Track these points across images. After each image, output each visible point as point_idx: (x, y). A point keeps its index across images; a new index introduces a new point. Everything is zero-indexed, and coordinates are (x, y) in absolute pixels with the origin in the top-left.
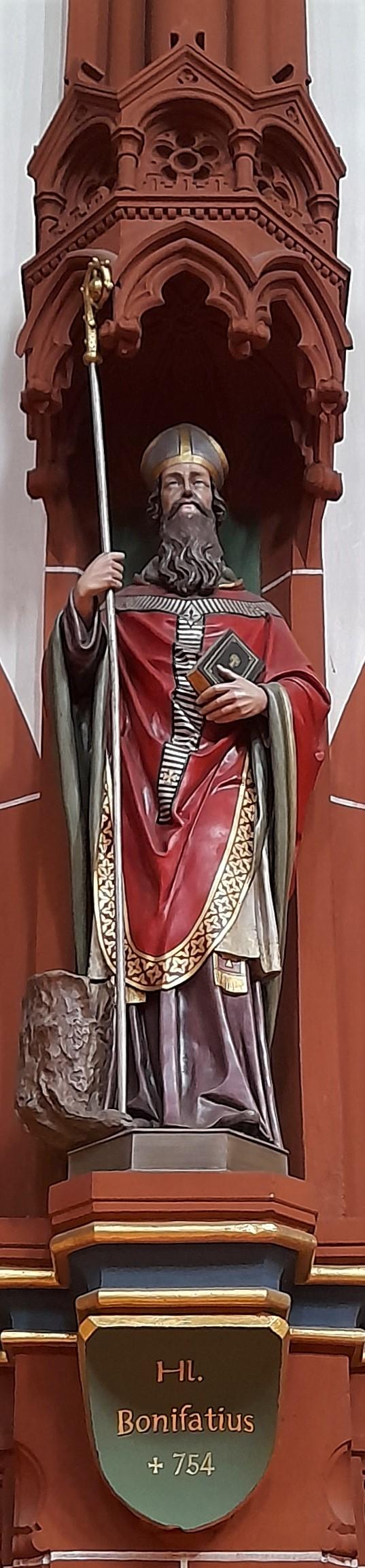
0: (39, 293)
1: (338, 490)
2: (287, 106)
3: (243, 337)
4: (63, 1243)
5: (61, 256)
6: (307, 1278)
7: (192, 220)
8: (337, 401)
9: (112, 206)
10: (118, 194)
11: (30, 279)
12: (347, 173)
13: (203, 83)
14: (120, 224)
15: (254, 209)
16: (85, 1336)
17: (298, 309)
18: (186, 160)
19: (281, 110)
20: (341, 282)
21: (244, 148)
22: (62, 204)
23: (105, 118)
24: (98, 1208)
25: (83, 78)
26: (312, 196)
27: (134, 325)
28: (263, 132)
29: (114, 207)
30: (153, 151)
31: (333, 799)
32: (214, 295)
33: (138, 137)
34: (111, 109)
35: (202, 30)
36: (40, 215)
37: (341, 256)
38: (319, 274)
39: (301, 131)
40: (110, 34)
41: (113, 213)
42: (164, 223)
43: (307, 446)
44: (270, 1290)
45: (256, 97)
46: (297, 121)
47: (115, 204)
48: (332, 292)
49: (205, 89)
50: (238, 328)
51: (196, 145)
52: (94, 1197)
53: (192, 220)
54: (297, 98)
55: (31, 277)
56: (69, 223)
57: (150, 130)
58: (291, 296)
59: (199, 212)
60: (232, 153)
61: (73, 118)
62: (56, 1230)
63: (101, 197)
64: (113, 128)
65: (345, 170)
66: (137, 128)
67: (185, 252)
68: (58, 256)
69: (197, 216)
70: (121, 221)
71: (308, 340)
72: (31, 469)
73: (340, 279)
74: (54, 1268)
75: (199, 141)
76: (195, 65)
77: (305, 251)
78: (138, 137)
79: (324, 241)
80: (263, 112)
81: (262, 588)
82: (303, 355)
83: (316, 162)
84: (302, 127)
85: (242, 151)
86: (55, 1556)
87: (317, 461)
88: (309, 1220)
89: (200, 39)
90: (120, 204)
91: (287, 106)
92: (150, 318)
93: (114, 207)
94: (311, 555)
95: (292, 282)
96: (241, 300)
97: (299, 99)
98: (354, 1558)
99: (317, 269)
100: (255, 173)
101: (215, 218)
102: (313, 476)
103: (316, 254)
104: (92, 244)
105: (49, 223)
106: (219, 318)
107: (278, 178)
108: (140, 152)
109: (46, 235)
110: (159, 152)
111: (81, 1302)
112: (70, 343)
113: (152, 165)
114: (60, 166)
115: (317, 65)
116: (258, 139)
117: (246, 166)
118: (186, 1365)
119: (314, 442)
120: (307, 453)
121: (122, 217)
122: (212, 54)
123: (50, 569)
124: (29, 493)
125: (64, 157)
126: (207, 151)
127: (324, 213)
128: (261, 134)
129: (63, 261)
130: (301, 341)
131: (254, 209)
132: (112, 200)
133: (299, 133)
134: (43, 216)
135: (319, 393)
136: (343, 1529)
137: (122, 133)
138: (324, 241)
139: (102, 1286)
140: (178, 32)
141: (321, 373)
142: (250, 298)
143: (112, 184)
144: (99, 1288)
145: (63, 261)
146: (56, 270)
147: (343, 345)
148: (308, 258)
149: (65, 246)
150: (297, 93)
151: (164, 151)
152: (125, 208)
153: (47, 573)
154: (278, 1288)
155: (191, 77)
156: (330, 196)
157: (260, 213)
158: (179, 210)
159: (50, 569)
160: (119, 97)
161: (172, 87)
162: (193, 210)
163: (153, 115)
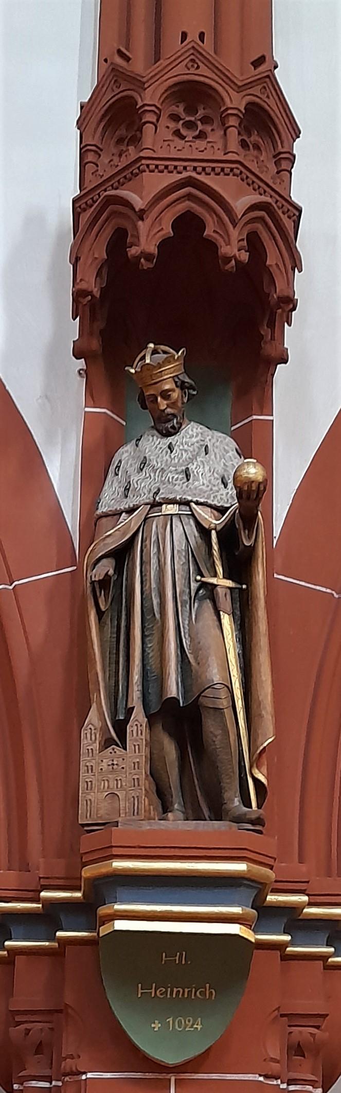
0: (85, 218)
1: (286, 358)
2: (260, 87)
3: (228, 260)
4: (88, 872)
5: (101, 194)
6: (264, 902)
7: (194, 174)
8: (289, 303)
9: (138, 162)
10: (142, 154)
11: (78, 209)
12: (301, 135)
13: (204, 70)
14: (142, 176)
15: (238, 168)
16: (102, 933)
17: (265, 236)
18: (190, 125)
19: (256, 90)
20: (295, 217)
21: (233, 121)
22: (98, 153)
23: (136, 93)
24: (115, 851)
25: (118, 60)
26: (277, 152)
27: (153, 249)
28: (245, 109)
29: (140, 164)
30: (172, 135)
31: (276, 576)
32: (209, 232)
33: (157, 112)
34: (139, 87)
35: (204, 30)
36: (84, 161)
37: (295, 198)
38: (280, 212)
39: (271, 104)
40: (129, 12)
41: (138, 168)
42: (176, 177)
43: (267, 327)
44: (244, 907)
45: (240, 84)
46: (268, 97)
47: (140, 161)
48: (288, 224)
49: (204, 74)
50: (225, 253)
51: (198, 115)
52: (113, 844)
53: (194, 174)
54: (267, 80)
55: (80, 207)
56: (106, 170)
57: (164, 104)
58: (259, 227)
59: (199, 169)
60: (223, 124)
61: (109, 88)
62: (85, 864)
63: (130, 155)
64: (140, 104)
65: (300, 133)
66: (156, 104)
67: (189, 197)
68: (99, 194)
69: (198, 171)
70: (144, 173)
71: (272, 260)
72: (75, 339)
73: (294, 215)
74: (82, 892)
75: (201, 113)
76: (196, 57)
77: (271, 197)
78: (157, 112)
79: (285, 189)
80: (244, 93)
81: (232, 426)
82: (267, 269)
83: (280, 127)
84: (271, 102)
85: (231, 123)
86: (89, 1075)
87: (273, 338)
88: (271, 862)
89: (202, 36)
90: (143, 162)
91: (260, 87)
92: (163, 245)
93: (140, 164)
94: (266, 405)
95: (262, 219)
96: (228, 236)
97: (270, 82)
98: (278, 1079)
99: (279, 208)
100: (239, 134)
101: (210, 174)
102: (269, 350)
103: (279, 198)
104: (123, 187)
105: (90, 168)
106: (212, 246)
107: (255, 138)
108: (158, 120)
109: (88, 176)
110: (172, 119)
111: (103, 910)
112: (106, 257)
113: (167, 129)
114: (101, 120)
115: (280, 52)
116: (241, 115)
117: (233, 133)
118: (181, 955)
119: (272, 325)
120: (265, 331)
121: (145, 171)
122: (208, 46)
123: (87, 409)
124: (74, 355)
125: (104, 116)
126: (206, 120)
127: (284, 165)
128: (244, 111)
129: (102, 198)
130: (268, 261)
131: (238, 168)
132: (138, 158)
133: (269, 106)
134: (87, 161)
135: (278, 298)
136: (273, 1060)
137: (147, 108)
138: (285, 189)
139: (107, 902)
140: (187, 31)
141: (280, 285)
142: (234, 233)
143: (135, 140)
144: (116, 902)
145: (102, 198)
146: (97, 203)
147: (296, 263)
148: (273, 201)
149: (103, 188)
150: (268, 76)
151: (175, 118)
152: (148, 166)
153: (85, 412)
154: (250, 906)
155: (196, 66)
156: (289, 153)
157: (241, 173)
158: (185, 168)
159: (87, 409)
160: (144, 80)
161: (180, 72)
162: (195, 169)
163: (168, 92)
